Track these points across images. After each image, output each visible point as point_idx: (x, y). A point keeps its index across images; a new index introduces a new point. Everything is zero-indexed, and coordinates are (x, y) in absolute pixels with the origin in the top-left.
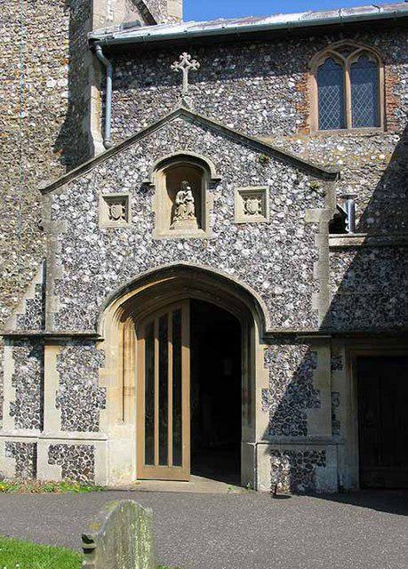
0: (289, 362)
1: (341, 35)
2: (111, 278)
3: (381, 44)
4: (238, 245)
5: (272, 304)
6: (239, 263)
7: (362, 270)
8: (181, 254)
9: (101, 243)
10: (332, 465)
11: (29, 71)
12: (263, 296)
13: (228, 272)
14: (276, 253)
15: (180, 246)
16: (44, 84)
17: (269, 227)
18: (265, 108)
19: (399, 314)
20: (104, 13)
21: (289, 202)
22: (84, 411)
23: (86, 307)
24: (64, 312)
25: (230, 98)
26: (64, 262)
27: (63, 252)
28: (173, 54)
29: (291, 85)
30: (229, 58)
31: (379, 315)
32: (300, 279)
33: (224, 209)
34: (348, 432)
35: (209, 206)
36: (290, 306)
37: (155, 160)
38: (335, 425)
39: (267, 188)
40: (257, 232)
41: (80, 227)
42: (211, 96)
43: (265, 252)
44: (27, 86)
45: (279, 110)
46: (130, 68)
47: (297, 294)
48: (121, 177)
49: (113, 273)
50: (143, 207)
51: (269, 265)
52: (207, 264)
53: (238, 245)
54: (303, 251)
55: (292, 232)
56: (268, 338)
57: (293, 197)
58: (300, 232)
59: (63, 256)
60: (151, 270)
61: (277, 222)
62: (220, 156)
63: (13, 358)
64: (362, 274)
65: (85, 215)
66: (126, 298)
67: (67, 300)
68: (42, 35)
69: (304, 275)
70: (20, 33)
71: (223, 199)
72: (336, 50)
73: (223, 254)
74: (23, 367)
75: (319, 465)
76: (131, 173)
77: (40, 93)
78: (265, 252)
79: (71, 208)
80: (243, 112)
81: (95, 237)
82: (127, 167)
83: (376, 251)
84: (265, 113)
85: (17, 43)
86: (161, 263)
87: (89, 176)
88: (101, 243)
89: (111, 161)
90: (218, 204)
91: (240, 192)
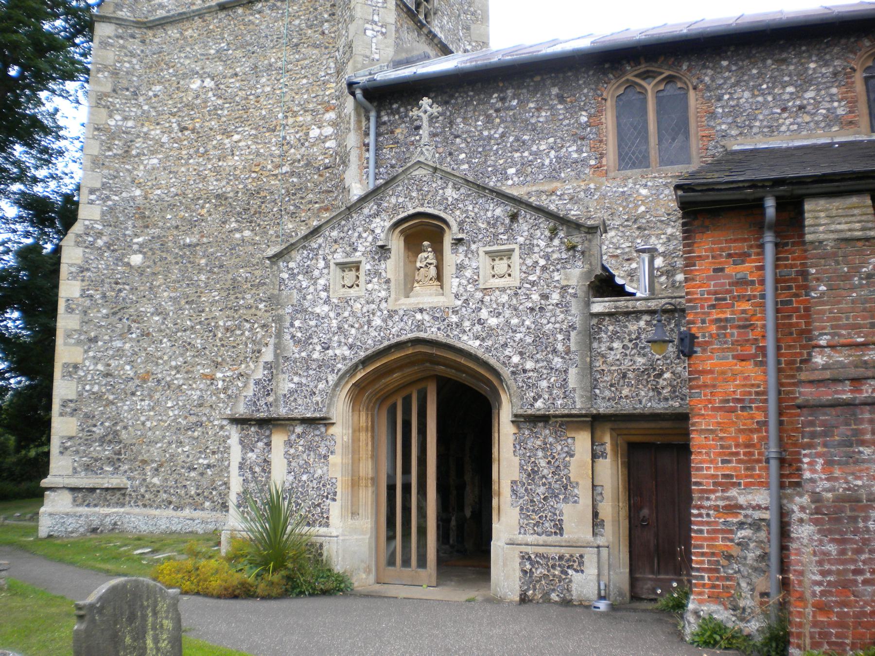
0: (543, 449)
1: (642, 61)
2: (343, 353)
3: (689, 69)
4: (484, 314)
5: (523, 381)
6: (484, 335)
7: (630, 341)
8: (419, 326)
9: (332, 315)
10: (591, 570)
11: (290, 121)
12: (513, 373)
13: (471, 344)
14: (527, 323)
15: (419, 316)
16: (307, 134)
17: (519, 291)
18: (552, 148)
19: (675, 392)
20: (368, 53)
21: (542, 262)
22: (313, 503)
23: (316, 387)
24: (292, 392)
25: (511, 139)
26: (293, 337)
27: (292, 325)
28: (446, 93)
29: (584, 119)
30: (510, 92)
31: (651, 394)
32: (555, 351)
33: (468, 273)
34: (614, 534)
35: (449, 269)
36: (544, 384)
37: (391, 219)
38: (596, 521)
39: (516, 247)
40: (504, 298)
41: (309, 297)
42: (490, 138)
43: (515, 321)
44: (288, 138)
45: (570, 149)
46: (398, 112)
47: (552, 369)
48: (353, 240)
49: (345, 348)
50: (377, 274)
51: (519, 336)
52: (448, 335)
53: (484, 314)
54: (559, 319)
55: (545, 297)
56: (529, 421)
57: (547, 257)
58: (555, 297)
59: (292, 330)
60: (386, 343)
61: (529, 286)
62: (463, 212)
63: (241, 444)
64: (630, 345)
65: (315, 284)
66: (359, 376)
67: (296, 379)
68: (304, 81)
69: (560, 347)
70: (282, 81)
71: (466, 262)
72: (636, 76)
73: (467, 324)
74: (250, 455)
75: (577, 571)
76: (364, 235)
77: (303, 144)
78: (515, 321)
79: (300, 277)
80: (526, 154)
81: (326, 308)
82: (361, 229)
83: (647, 317)
84: (553, 154)
85: (278, 92)
86: (398, 336)
87: (320, 240)
88: (332, 315)
89: (343, 222)
90: (460, 267)
91: (486, 253)
